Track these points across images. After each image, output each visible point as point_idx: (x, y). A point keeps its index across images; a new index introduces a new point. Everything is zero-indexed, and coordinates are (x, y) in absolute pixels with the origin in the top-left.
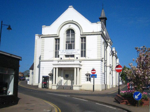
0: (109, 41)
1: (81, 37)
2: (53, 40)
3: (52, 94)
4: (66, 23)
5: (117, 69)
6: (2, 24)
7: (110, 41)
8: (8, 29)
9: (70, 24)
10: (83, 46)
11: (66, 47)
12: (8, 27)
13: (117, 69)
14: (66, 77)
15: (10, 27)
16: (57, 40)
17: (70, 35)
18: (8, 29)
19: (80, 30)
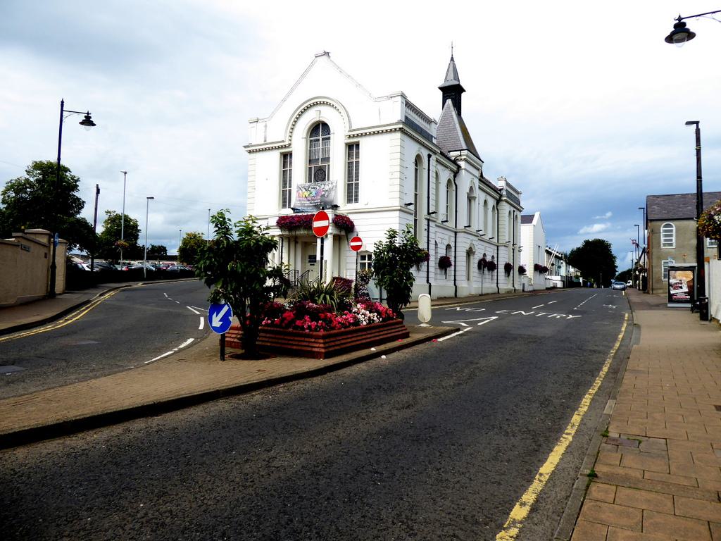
0: (464, 155)
1: (346, 144)
2: (275, 157)
3: (162, 356)
4: (306, 105)
5: (358, 244)
6: (62, 110)
7: (467, 156)
8: (82, 123)
9: (319, 108)
10: (352, 171)
11: (310, 175)
12: (82, 118)
13: (358, 244)
14: (309, 262)
15: (90, 117)
16: (286, 157)
17: (321, 140)
18: (82, 123)
19: (295, 122)
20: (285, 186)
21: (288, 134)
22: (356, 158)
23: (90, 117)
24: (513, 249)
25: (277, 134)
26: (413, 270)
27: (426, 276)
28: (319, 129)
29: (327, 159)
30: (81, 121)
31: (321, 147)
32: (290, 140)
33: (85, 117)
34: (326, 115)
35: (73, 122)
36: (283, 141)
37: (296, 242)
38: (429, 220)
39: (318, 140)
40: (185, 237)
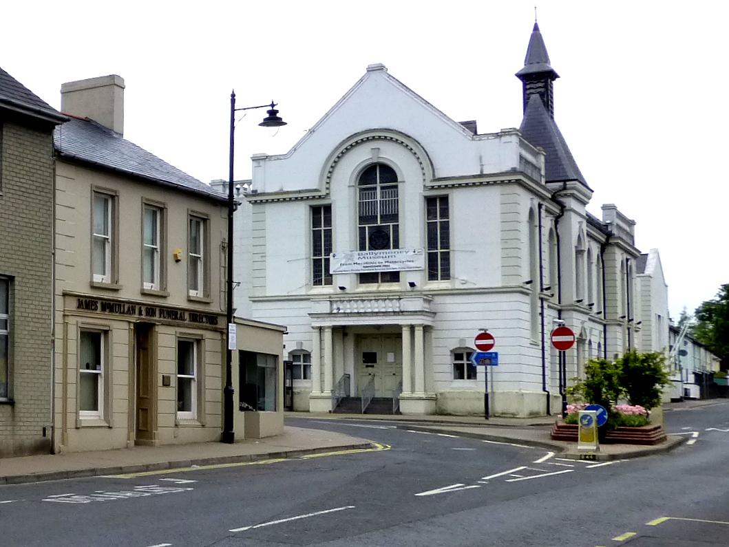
2: (300, 216)
14: (364, 362)
16: (321, 214)
17: (378, 189)
20: (317, 250)
21: (325, 180)
22: (442, 217)
23: (277, 112)
24: (629, 329)
25: (306, 178)
26: (108, 310)
27: (541, 373)
28: (378, 176)
29: (395, 217)
30: (262, 121)
31: (379, 198)
32: (327, 189)
33: (269, 112)
34: (392, 155)
35: (249, 124)
36: (316, 190)
37: (345, 335)
38: (542, 300)
39: (375, 188)
40: (287, 359)
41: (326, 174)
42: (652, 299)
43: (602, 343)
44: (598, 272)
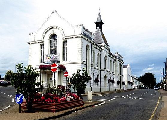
2: (38, 46)
16: (42, 46)
17: (54, 40)
20: (41, 55)
21: (43, 38)
25: (39, 38)
26: (86, 83)
28: (54, 37)
34: (56, 32)
37: (45, 74)
38: (91, 66)
39: (53, 40)
41: (43, 35)
42: (58, 39)
43: (99, 75)
44: (114, 65)
